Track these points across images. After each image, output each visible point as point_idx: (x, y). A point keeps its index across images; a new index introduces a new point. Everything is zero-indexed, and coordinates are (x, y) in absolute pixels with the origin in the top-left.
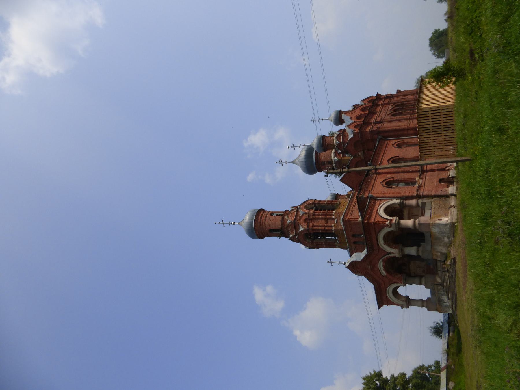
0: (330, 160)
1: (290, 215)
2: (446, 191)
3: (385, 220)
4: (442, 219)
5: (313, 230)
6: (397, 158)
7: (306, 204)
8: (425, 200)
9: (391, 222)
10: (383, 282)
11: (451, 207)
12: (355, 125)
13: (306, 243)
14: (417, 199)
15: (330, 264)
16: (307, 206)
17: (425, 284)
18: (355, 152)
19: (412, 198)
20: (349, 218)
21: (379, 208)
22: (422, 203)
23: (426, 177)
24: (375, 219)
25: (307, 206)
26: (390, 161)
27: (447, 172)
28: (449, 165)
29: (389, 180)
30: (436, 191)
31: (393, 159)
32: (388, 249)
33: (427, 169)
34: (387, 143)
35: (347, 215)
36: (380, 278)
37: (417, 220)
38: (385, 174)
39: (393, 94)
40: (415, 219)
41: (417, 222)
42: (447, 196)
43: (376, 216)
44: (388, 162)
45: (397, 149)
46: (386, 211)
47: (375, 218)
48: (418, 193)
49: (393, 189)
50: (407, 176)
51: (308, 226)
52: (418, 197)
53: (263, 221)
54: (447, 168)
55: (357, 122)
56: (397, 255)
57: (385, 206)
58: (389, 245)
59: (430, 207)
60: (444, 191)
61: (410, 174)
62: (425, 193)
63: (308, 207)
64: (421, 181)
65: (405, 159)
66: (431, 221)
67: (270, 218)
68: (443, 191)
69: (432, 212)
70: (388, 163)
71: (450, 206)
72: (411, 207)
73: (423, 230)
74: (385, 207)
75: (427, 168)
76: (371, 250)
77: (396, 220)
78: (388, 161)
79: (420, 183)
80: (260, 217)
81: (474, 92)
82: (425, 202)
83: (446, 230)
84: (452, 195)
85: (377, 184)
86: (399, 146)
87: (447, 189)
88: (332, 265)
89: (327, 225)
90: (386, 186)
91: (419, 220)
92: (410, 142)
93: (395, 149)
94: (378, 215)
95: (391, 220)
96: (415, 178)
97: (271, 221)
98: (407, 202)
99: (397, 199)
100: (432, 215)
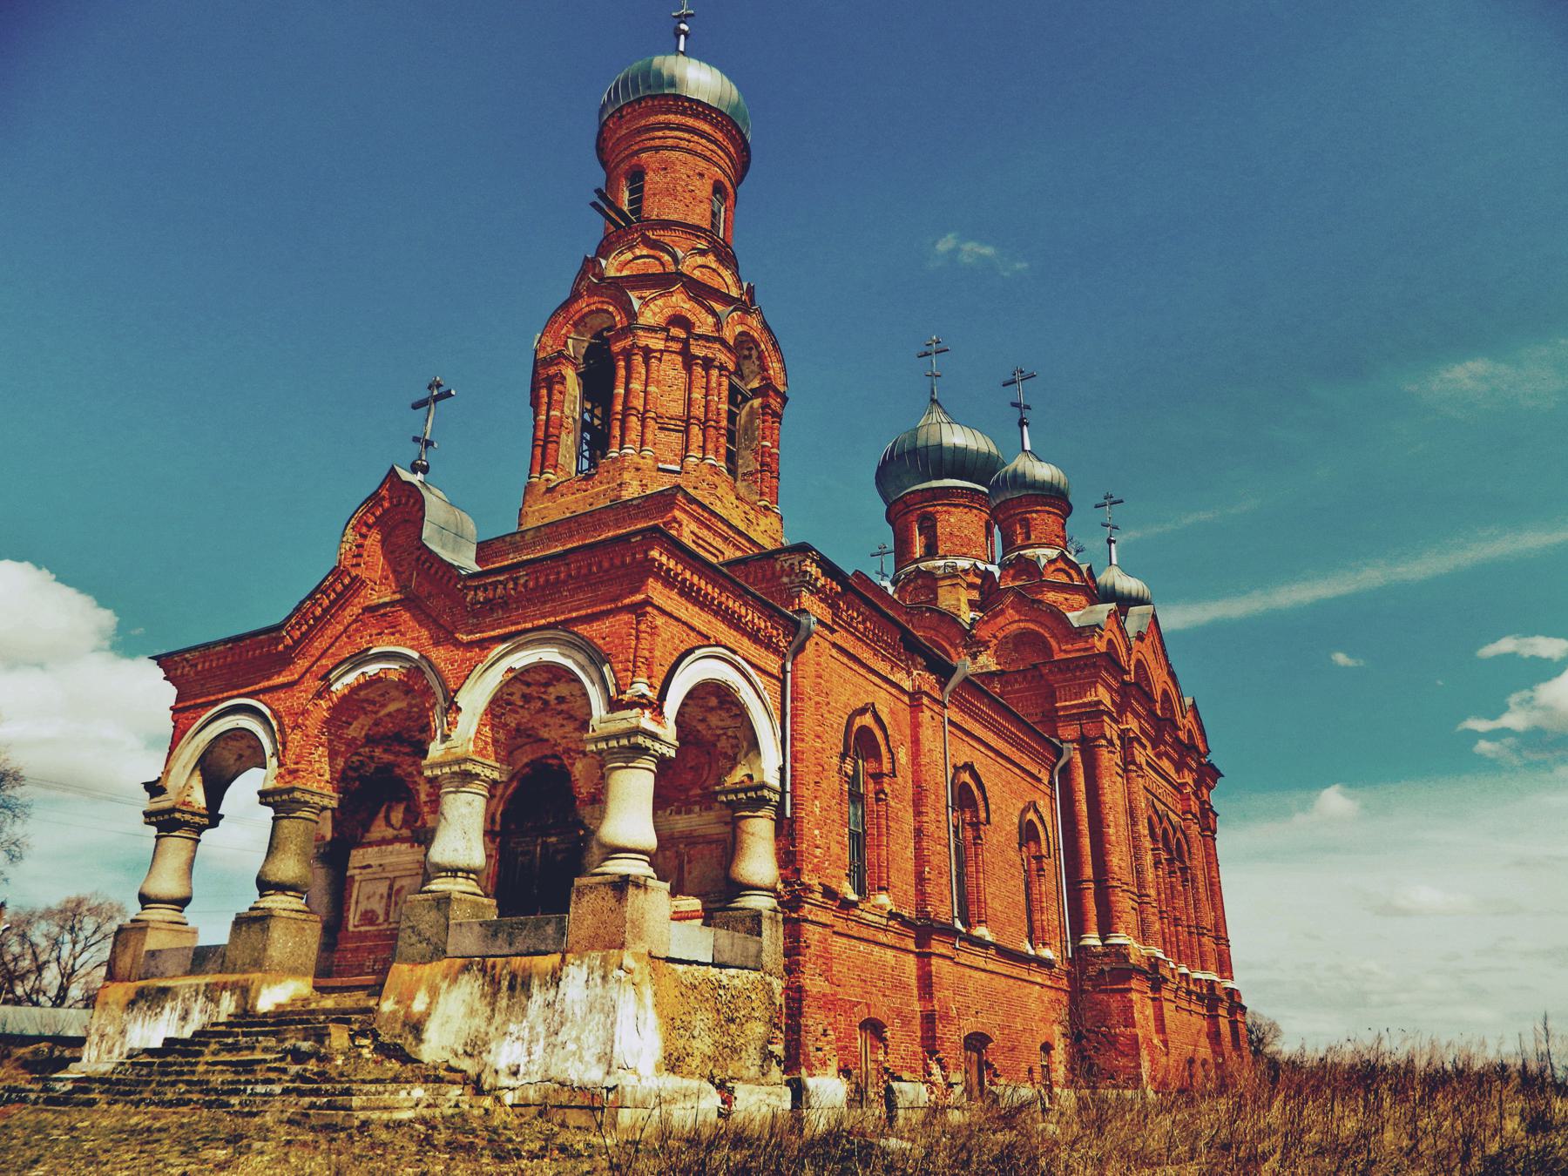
0: (941, 552)
1: (714, 265)
2: (824, 1064)
3: (662, 677)
4: (1159, 692)
5: (628, 354)
6: (983, 815)
7: (763, 346)
8: (772, 939)
9: (643, 707)
10: (296, 676)
11: (723, 1087)
12: (1115, 641)
13: (563, 332)
14: (780, 886)
15: (425, 394)
16: (754, 353)
17: (255, 913)
18: (995, 637)
19: (788, 858)
20: (681, 525)
21: (738, 658)
22: (757, 916)
23: (893, 947)
24: (670, 615)
25: (754, 353)
26: (966, 777)
27: (919, 1065)
28: (954, 1081)
29: (883, 748)
30: (829, 1004)
31: (976, 792)
32: (475, 696)
33: (934, 961)
34: (1039, 780)
35: (697, 520)
36: (319, 659)
37: (650, 872)
38: (909, 739)
39: (1215, 839)
40: (653, 859)
41: (638, 868)
42: (794, 1061)
43: (692, 629)
44: (966, 764)
45: (1016, 821)
46: (712, 695)
47: (678, 619)
48: (812, 892)
49: (836, 760)
50: (901, 850)
51: (650, 329)
52: (791, 899)
53: (689, 141)
54: (936, 1069)
55: (1129, 661)
56: (436, 750)
57: (746, 695)
58: (498, 706)
59: (726, 957)
60: (819, 1049)
61: (910, 866)
62: (812, 934)
63: (750, 356)
64: (876, 919)
65: (977, 855)
66: (637, 957)
67: (701, 175)
68: (819, 1044)
69: (700, 971)
70: (960, 764)
71: (729, 1084)
72: (731, 847)
73: (584, 912)
74: (742, 693)
75: (940, 961)
76: (481, 596)
77: (654, 737)
78: (969, 767)
79: (864, 915)
80: (706, 128)
81: (369, 907)
82: (760, 934)
83: (574, 1054)
84: (799, 1092)
85: (861, 680)
86: (1028, 833)
87: (834, 1066)
88: (416, 406)
89: (651, 423)
90: (855, 728)
91: (650, 882)
92: (1044, 888)
93: (1017, 813)
94: (694, 640)
95: (657, 708)
96: (887, 890)
97: (684, 177)
98: (760, 833)
99: (782, 770)
100: (680, 968)
